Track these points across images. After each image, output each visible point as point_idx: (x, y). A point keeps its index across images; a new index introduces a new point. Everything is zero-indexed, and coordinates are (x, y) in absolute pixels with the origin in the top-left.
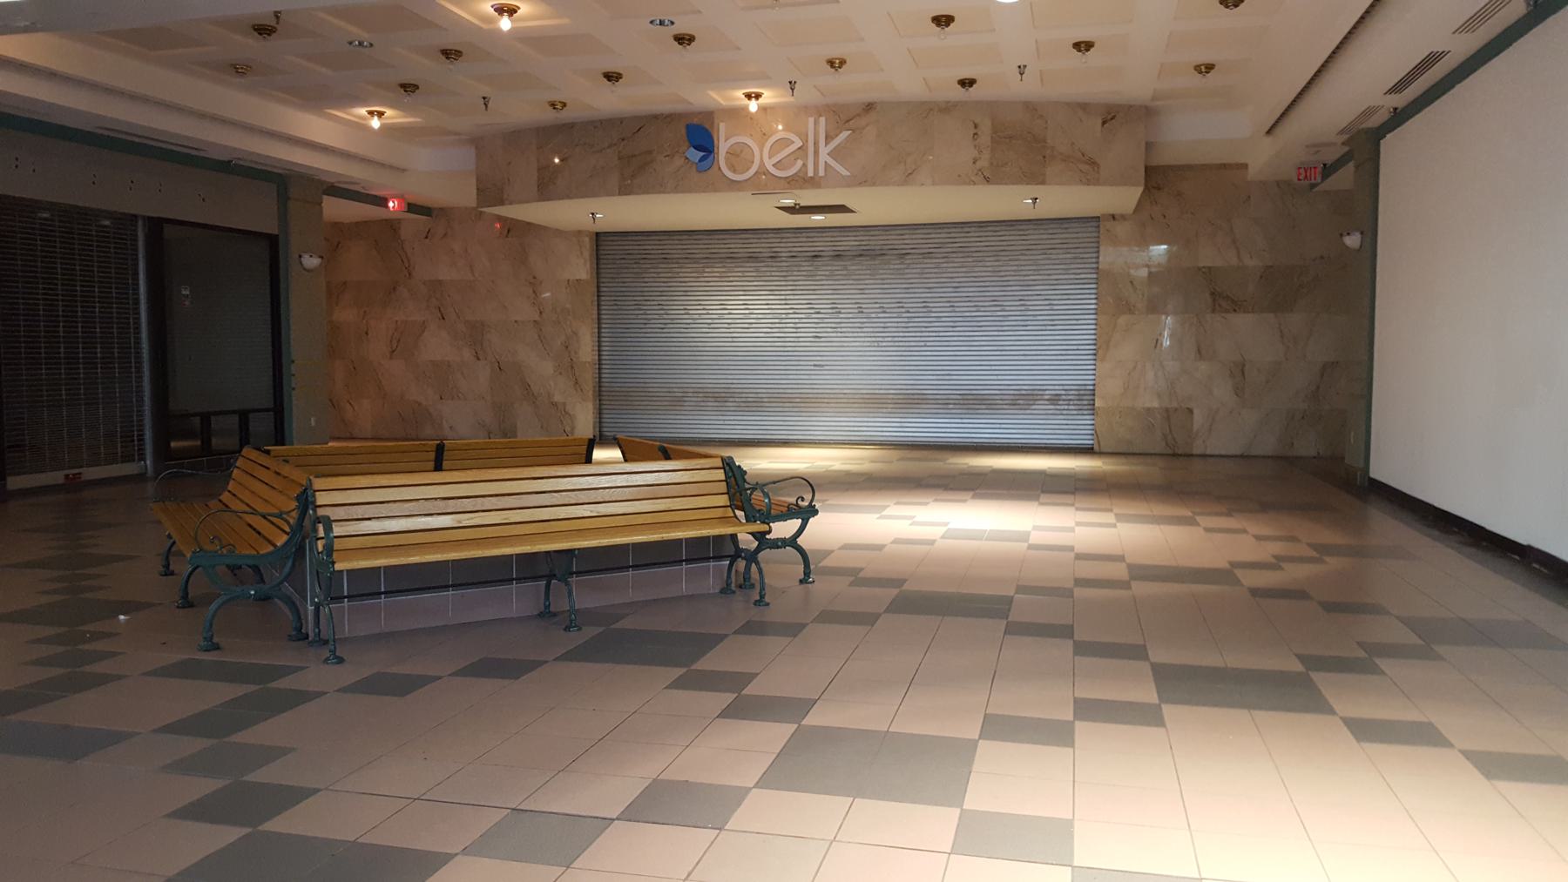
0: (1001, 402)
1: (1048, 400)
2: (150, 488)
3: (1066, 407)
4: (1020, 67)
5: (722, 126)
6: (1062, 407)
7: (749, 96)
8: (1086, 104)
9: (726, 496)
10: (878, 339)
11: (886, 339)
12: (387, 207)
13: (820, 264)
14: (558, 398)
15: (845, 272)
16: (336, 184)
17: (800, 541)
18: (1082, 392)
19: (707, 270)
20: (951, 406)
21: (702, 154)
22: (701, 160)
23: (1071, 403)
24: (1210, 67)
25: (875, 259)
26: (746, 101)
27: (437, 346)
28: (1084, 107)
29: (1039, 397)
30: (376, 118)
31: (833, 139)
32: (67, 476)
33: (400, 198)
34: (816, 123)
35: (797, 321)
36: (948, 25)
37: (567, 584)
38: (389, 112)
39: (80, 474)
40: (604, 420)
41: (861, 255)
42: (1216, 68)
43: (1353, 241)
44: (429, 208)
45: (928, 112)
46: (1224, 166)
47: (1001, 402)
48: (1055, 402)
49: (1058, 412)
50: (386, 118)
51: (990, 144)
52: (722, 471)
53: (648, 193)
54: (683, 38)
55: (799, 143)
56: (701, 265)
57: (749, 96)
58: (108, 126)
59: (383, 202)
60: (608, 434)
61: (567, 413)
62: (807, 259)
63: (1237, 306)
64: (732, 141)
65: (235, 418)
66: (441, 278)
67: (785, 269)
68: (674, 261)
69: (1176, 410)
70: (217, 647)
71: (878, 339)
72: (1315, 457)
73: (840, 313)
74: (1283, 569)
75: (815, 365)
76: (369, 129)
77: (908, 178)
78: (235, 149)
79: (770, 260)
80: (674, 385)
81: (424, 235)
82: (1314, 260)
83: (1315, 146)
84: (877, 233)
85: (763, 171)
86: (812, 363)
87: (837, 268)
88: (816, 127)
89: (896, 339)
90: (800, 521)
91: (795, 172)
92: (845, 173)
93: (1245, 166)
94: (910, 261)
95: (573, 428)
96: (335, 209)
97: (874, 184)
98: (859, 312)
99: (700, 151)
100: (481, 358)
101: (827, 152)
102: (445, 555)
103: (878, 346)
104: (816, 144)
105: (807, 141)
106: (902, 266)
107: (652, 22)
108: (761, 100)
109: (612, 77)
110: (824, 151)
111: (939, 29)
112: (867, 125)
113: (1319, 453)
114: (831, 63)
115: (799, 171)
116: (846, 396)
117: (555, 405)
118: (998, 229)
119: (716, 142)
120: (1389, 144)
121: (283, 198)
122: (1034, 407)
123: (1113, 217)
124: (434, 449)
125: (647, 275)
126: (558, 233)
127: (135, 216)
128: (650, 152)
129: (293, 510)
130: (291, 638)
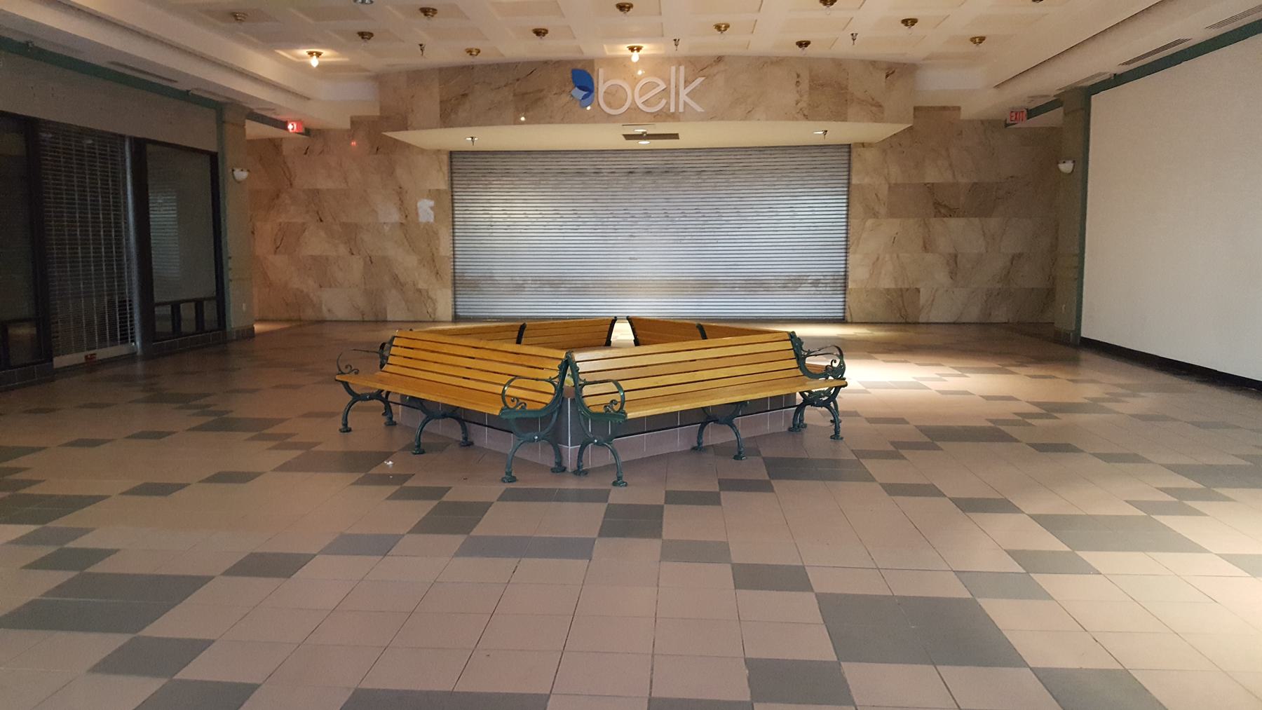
0: (775, 285)
1: (810, 283)
2: (139, 368)
3: (824, 289)
4: (852, 34)
5: (601, 71)
6: (821, 289)
7: (632, 49)
8: (875, 62)
9: (795, 361)
10: (680, 238)
11: (687, 238)
12: (286, 129)
13: (633, 178)
14: (421, 285)
15: (654, 185)
16: (256, 111)
17: (350, 398)
18: (836, 277)
19: (542, 182)
20: (737, 289)
21: (585, 93)
22: (585, 97)
23: (828, 285)
24: (982, 39)
25: (678, 175)
26: (629, 52)
27: (316, 244)
28: (874, 63)
29: (804, 281)
30: (315, 57)
31: (690, 83)
32: (86, 357)
33: (299, 122)
34: (677, 71)
35: (616, 223)
37: (732, 426)
38: (325, 53)
39: (95, 354)
40: (457, 303)
41: (666, 172)
42: (986, 40)
43: (1066, 167)
45: (765, 63)
46: (944, 108)
47: (775, 285)
48: (816, 285)
49: (818, 293)
50: (324, 57)
51: (808, 89)
52: (790, 342)
53: (539, 123)
54: (624, 7)
56: (537, 179)
57: (632, 49)
58: (136, 66)
59: (283, 125)
60: (461, 314)
61: (429, 298)
62: (623, 174)
63: (952, 212)
64: (609, 83)
65: (169, 308)
66: (319, 187)
67: (606, 182)
68: (516, 175)
69: (908, 289)
70: (513, 480)
71: (680, 238)
72: (1005, 323)
73: (650, 217)
75: (630, 258)
76: (308, 66)
77: (748, 115)
78: (198, 79)
79: (593, 175)
80: (516, 275)
81: (304, 151)
82: (1007, 179)
83: (1032, 97)
84: (680, 154)
86: (629, 256)
87: (494, 179)
88: (677, 74)
89: (694, 238)
91: (660, 108)
92: (699, 109)
93: (959, 108)
94: (706, 177)
95: (435, 310)
96: (254, 130)
97: (722, 119)
98: (666, 217)
99: (584, 90)
100: (354, 253)
101: (686, 93)
102: (693, 404)
103: (680, 243)
104: (677, 86)
105: (670, 84)
106: (700, 181)
108: (641, 52)
109: (541, 32)
110: (683, 93)
112: (717, 73)
113: (1009, 320)
114: (718, 27)
115: (631, 104)
116: (656, 282)
117: (419, 291)
118: (772, 152)
119: (595, 85)
120: (1096, 100)
121: (221, 122)
122: (800, 289)
123: (863, 145)
124: (518, 329)
125: (493, 186)
126: (422, 151)
127: (122, 137)
128: (541, 91)
130: (553, 470)
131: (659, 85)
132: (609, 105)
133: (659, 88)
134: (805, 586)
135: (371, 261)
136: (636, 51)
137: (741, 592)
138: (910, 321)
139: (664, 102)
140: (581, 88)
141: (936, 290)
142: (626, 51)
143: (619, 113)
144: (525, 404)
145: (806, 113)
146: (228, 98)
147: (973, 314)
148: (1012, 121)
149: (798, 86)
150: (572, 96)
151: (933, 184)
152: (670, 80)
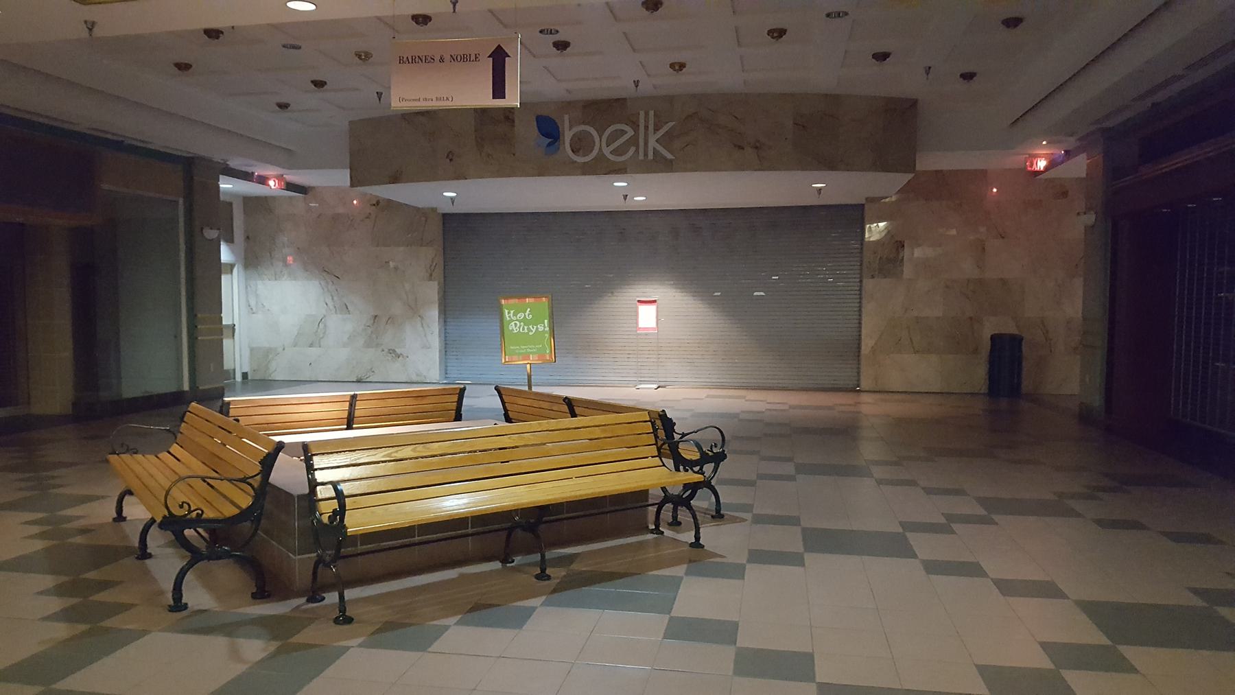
22: (549, 145)
36: (1016, 26)
44: (303, 187)
55: (631, 133)
74: (953, 532)
85: (601, 157)
90: (713, 464)
107: (541, 32)
111: (180, 72)
129: (258, 474)
131: (626, 132)
133: (626, 135)
134: (809, 676)
137: (806, 648)
139: (633, 149)
144: (202, 511)
146: (195, 154)
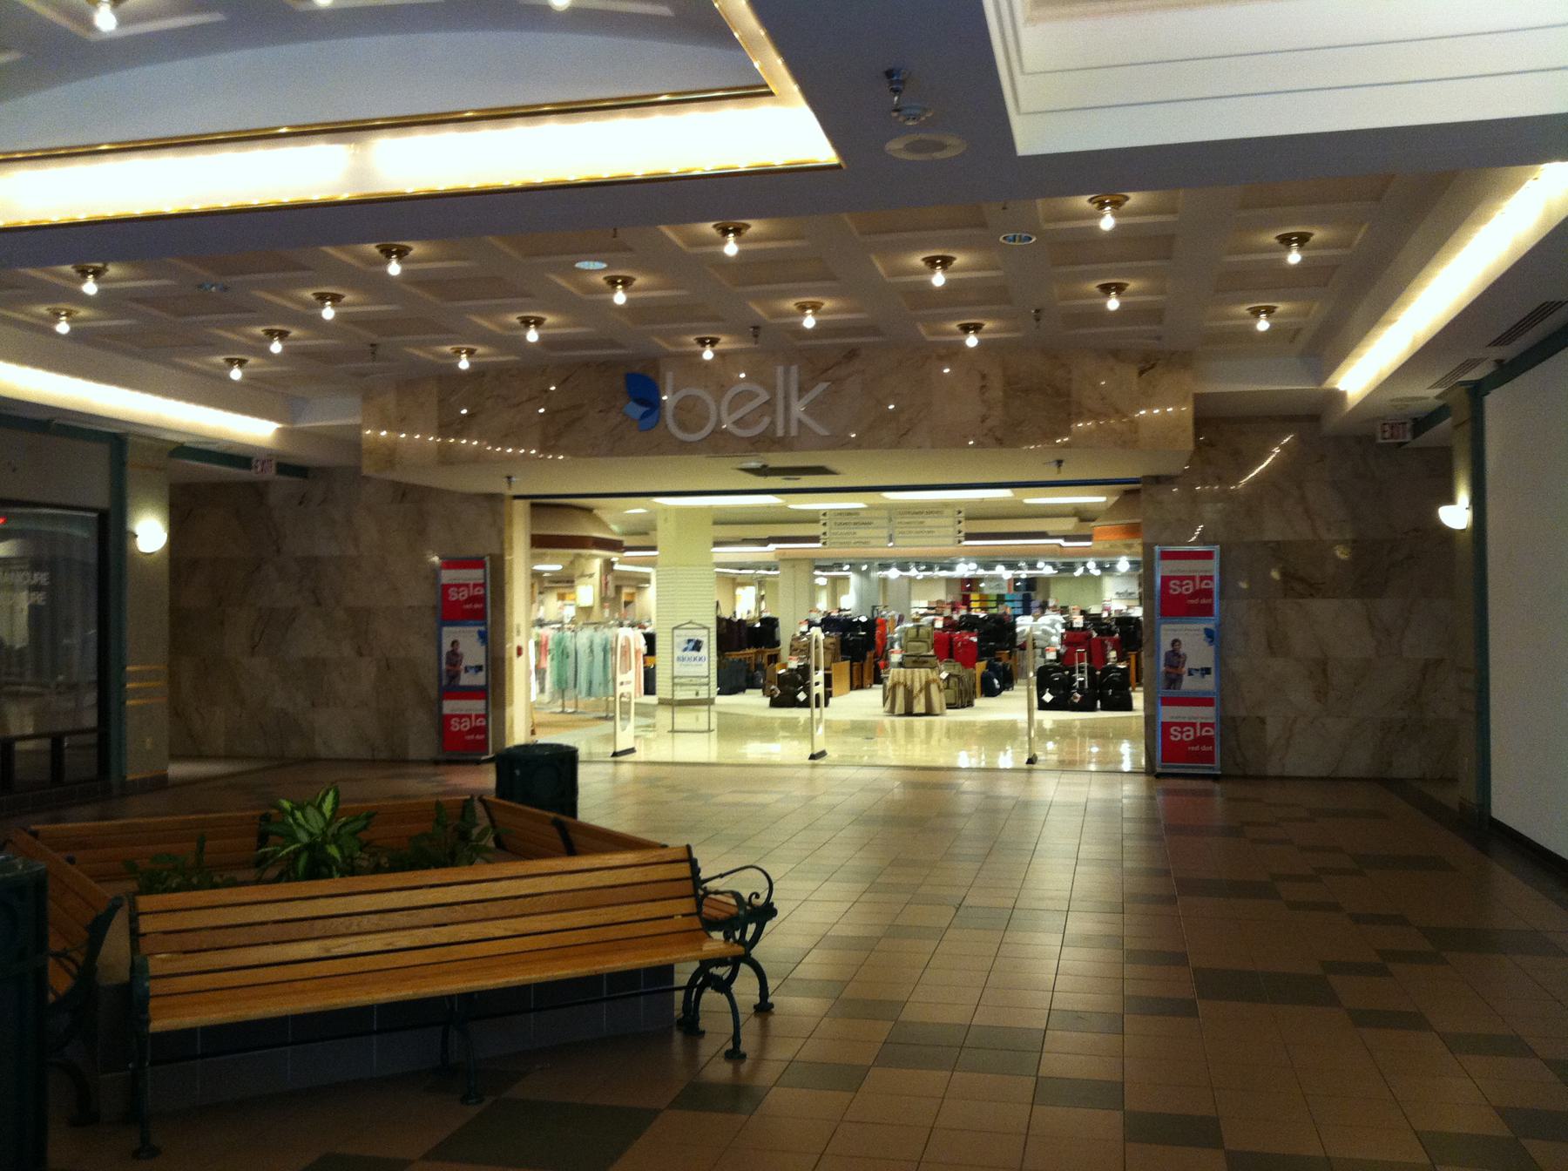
21: (645, 409)
22: (644, 416)
34: (787, 372)
110: (798, 408)
132: (683, 427)
135: (388, 666)
136: (708, 346)
138: (1290, 770)
139: (766, 420)
140: (641, 401)
141: (1295, 721)
142: (693, 345)
143: (703, 436)
145: (998, 434)
147: (1360, 761)
148: (1385, 439)
149: (983, 394)
150: (625, 415)
151: (1278, 543)
152: (775, 387)
